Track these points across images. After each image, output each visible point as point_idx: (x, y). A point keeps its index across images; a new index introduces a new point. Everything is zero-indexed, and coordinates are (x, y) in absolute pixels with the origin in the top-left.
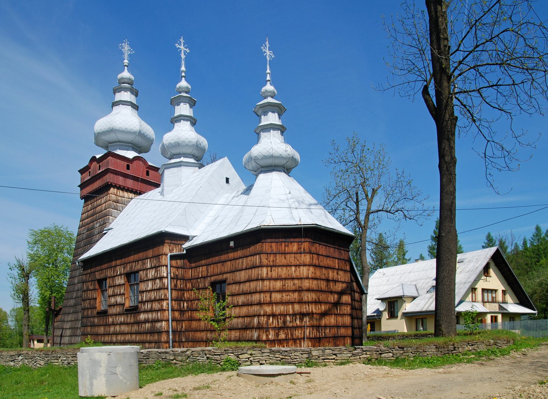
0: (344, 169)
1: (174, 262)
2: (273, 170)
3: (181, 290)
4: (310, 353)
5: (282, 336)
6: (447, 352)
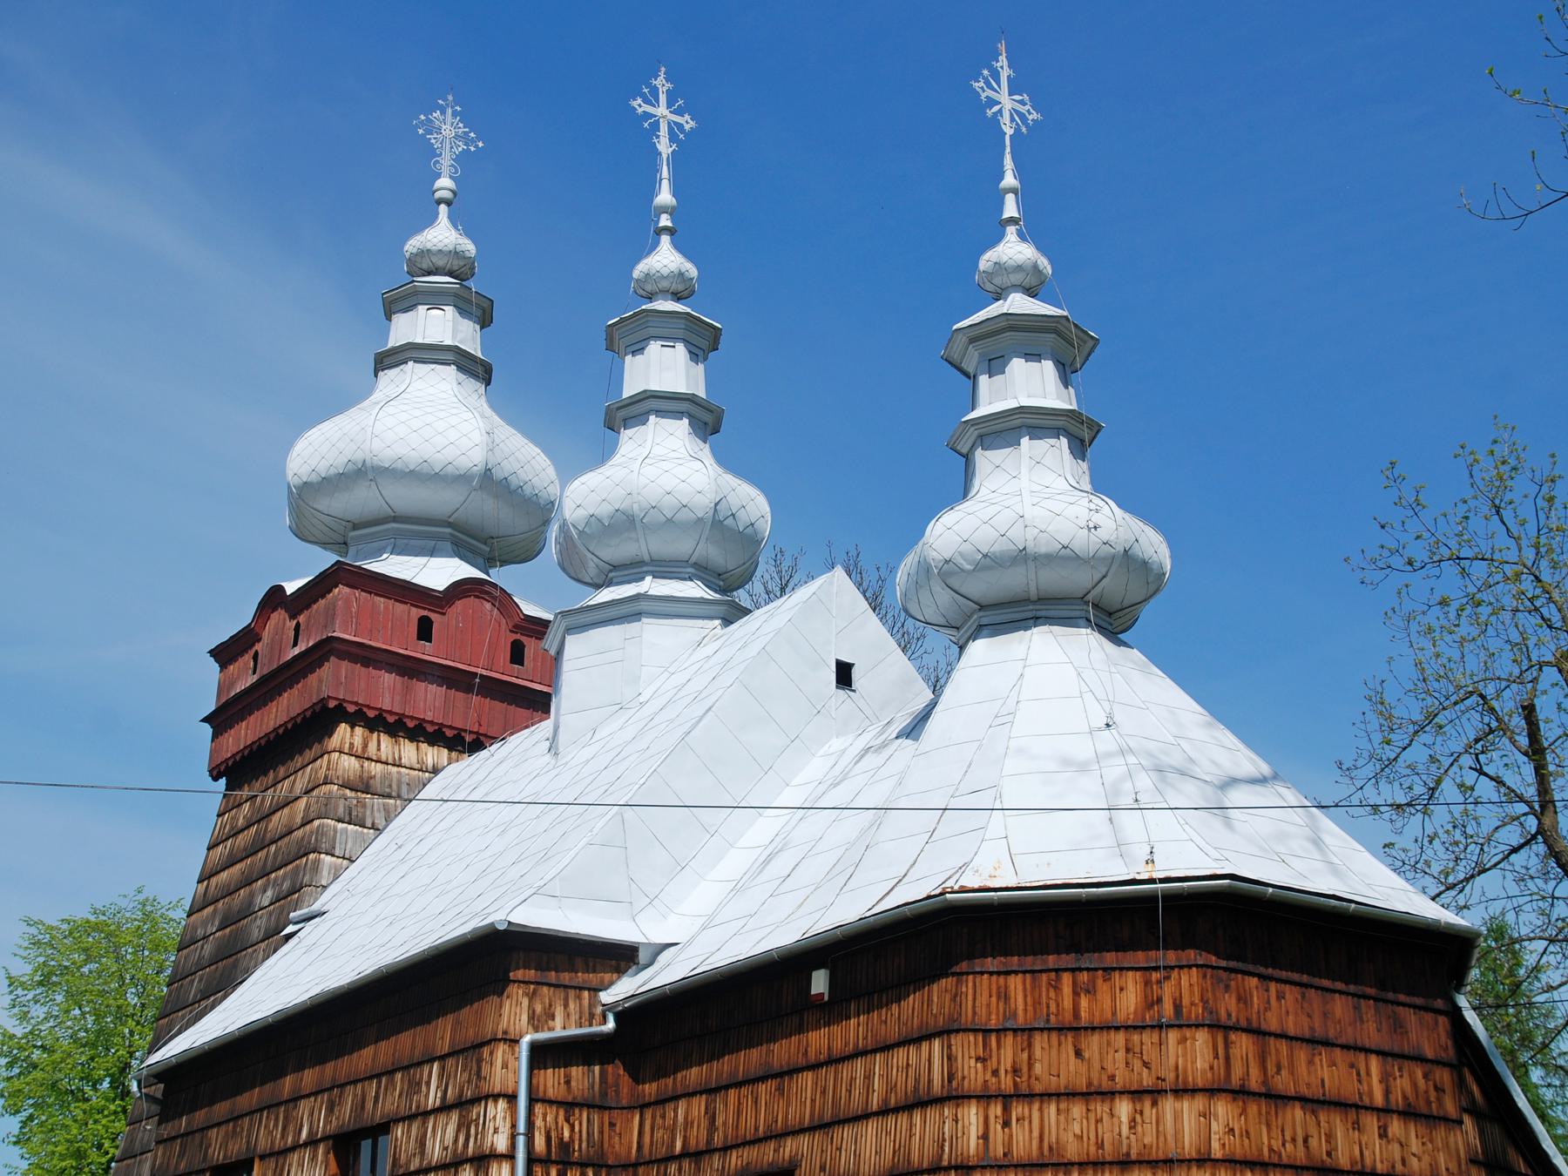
0: (1457, 596)
1: (551, 1080)
2: (1037, 620)
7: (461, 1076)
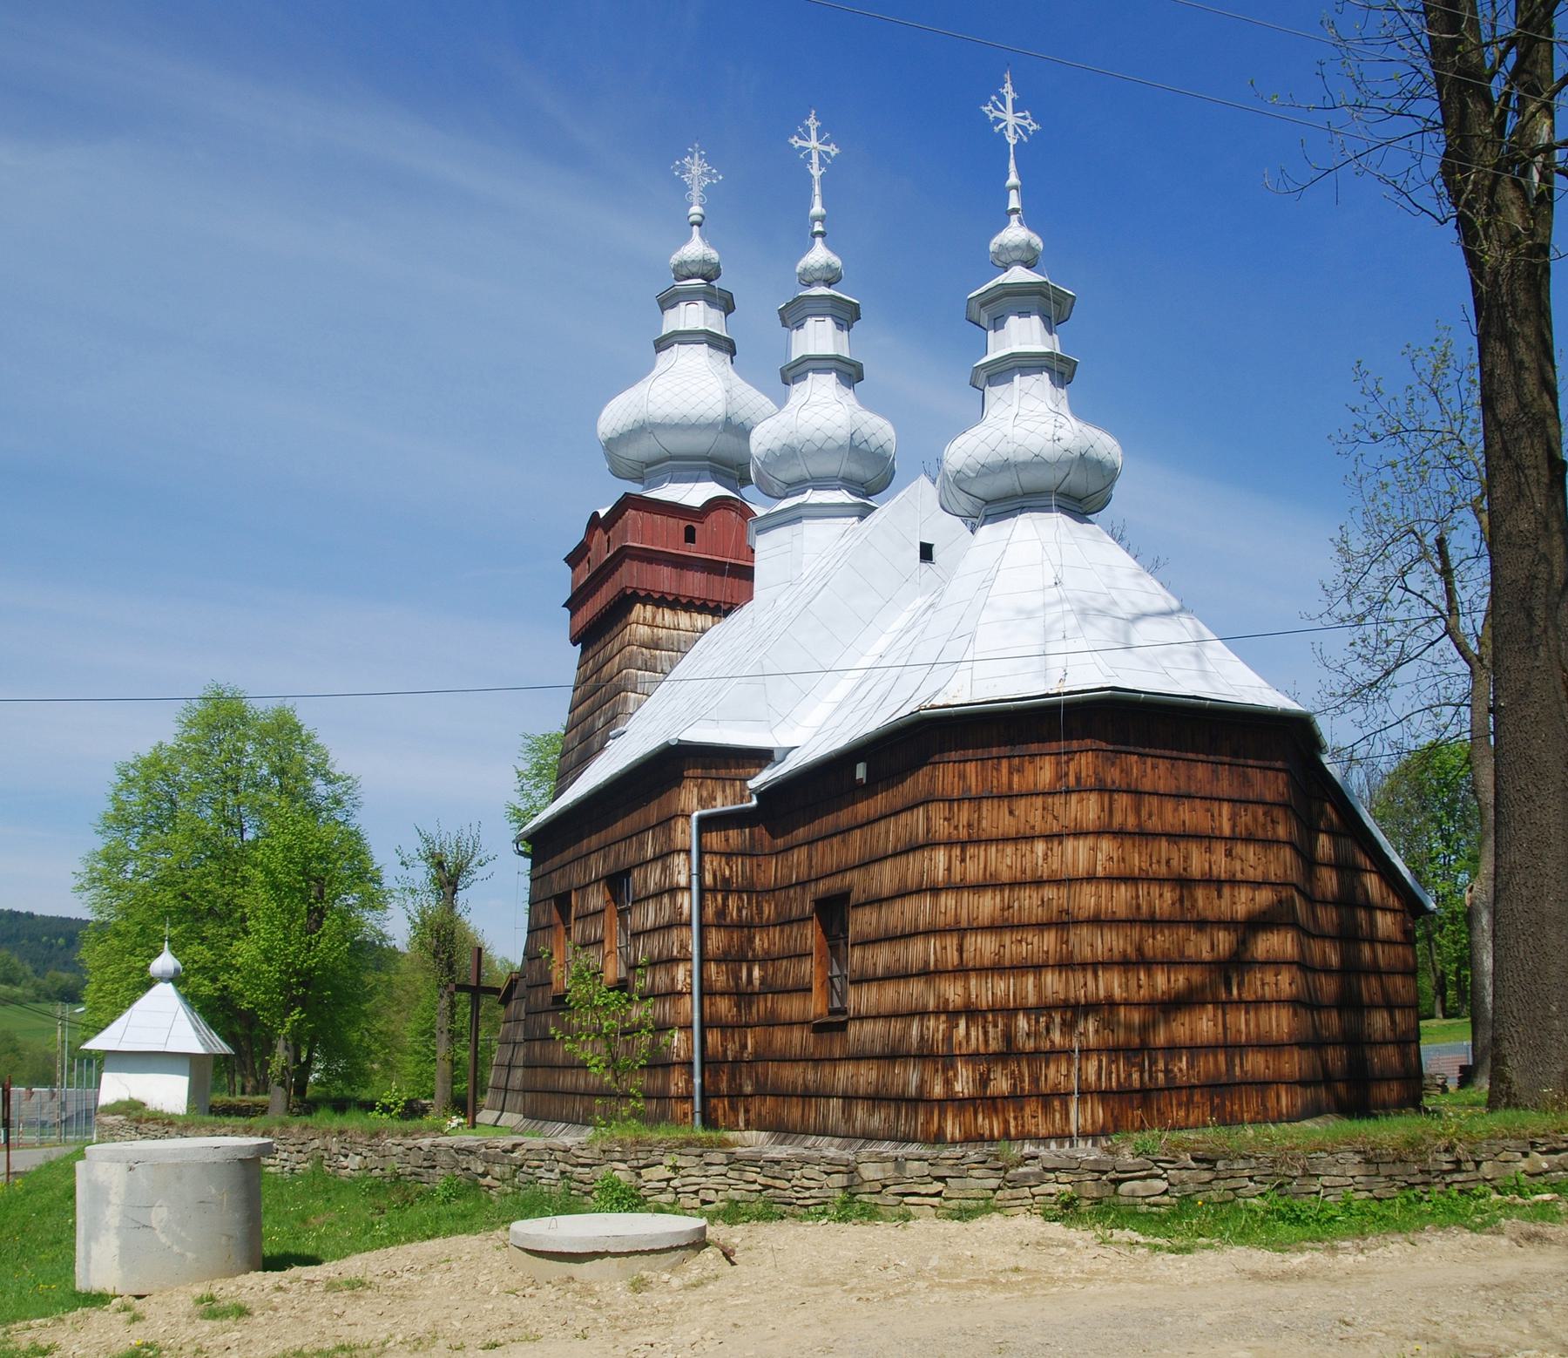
1: (715, 839)
2: (1022, 509)
3: (739, 926)
4: (852, 1171)
5: (1001, 1084)
6: (1419, 1178)
7: (662, 839)
